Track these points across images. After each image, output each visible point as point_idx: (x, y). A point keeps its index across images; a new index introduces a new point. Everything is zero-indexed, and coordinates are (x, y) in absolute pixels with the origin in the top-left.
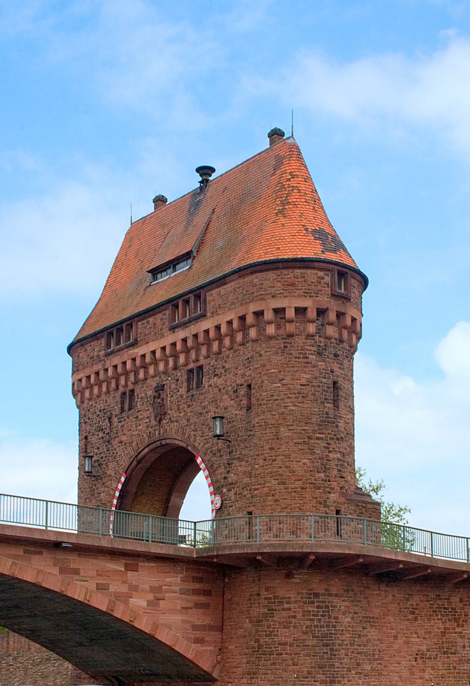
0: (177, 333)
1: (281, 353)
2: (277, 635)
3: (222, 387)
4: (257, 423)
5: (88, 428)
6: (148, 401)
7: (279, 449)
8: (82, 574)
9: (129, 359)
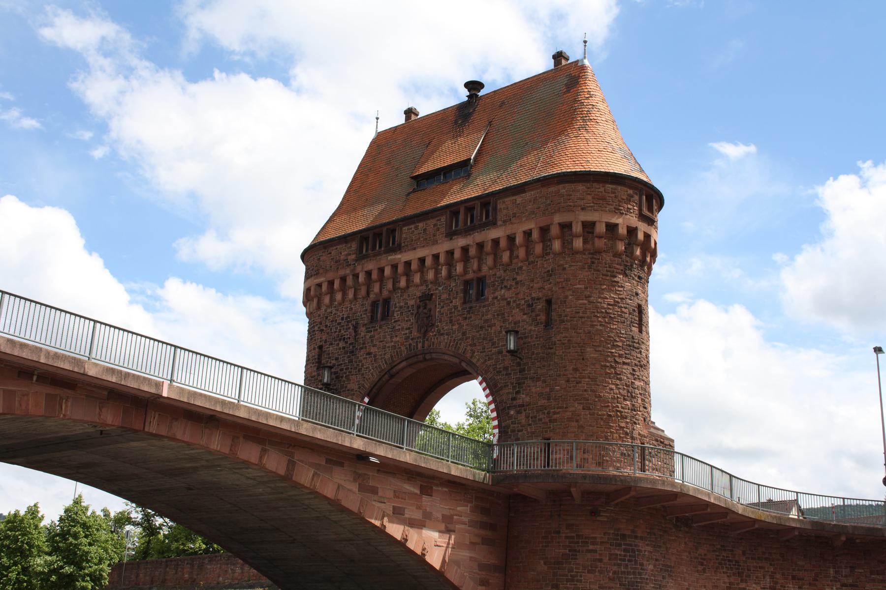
0: (456, 240)
1: (588, 268)
2: (581, 581)
3: (512, 300)
4: (558, 341)
5: (324, 337)
6: (410, 311)
7: (584, 370)
8: (380, 494)
9: (387, 265)
